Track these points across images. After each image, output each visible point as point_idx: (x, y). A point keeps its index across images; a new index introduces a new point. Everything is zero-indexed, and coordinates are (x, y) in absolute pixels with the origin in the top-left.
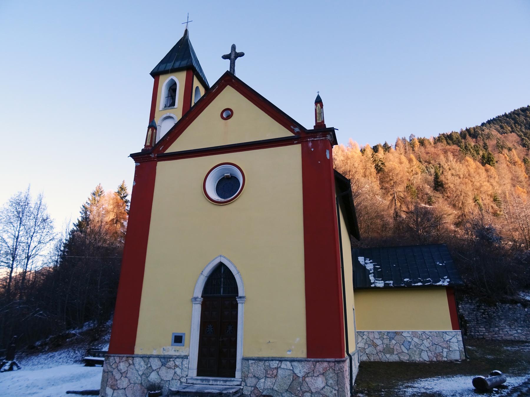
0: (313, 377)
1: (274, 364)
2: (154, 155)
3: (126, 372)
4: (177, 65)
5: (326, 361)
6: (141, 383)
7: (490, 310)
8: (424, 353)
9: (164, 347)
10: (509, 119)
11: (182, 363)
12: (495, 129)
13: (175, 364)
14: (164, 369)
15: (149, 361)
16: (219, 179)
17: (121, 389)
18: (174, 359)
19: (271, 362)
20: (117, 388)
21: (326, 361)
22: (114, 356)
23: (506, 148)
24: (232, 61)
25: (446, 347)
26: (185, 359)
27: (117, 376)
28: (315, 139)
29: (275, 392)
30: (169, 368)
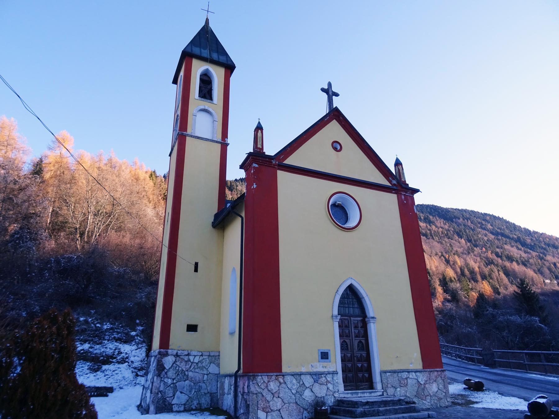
1: (405, 375)
2: (275, 162)
3: (278, 391)
9: (312, 364)
11: (332, 378)
13: (327, 380)
14: (316, 385)
17: (275, 411)
19: (402, 373)
22: (261, 376)
27: (269, 397)
30: (321, 385)
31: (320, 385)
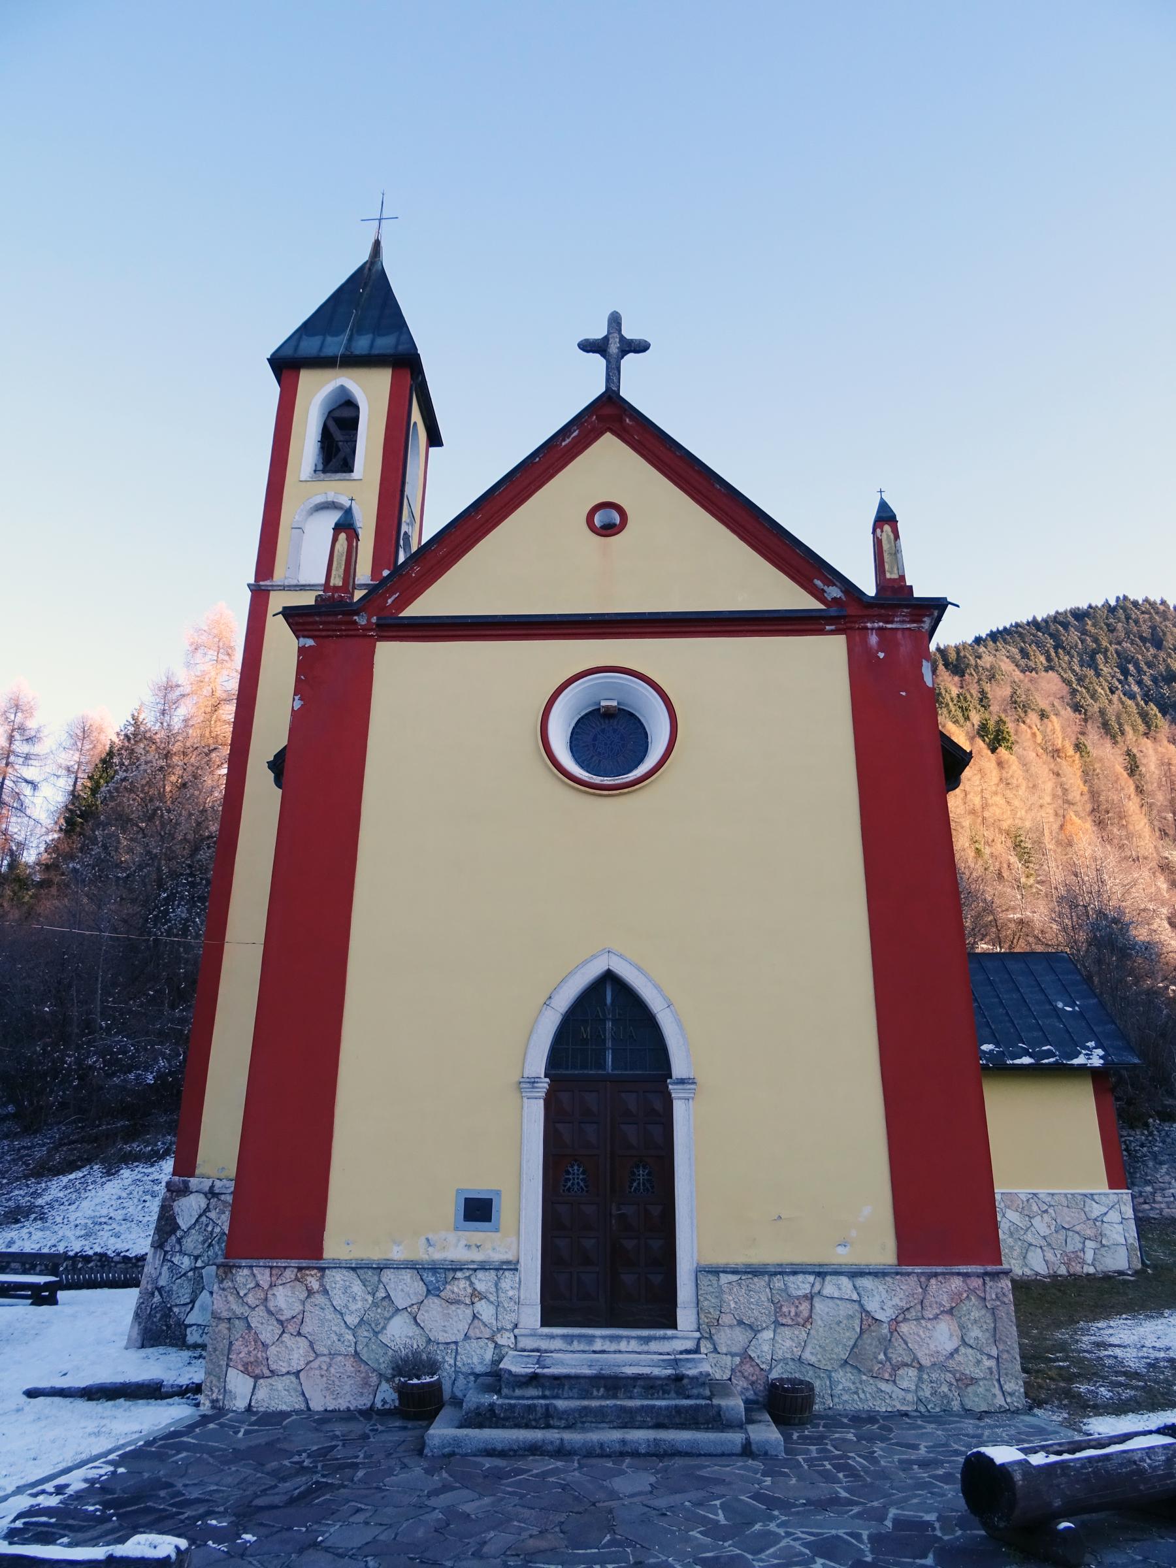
0: (922, 1321)
1: (801, 1285)
2: (369, 620)
3: (300, 1317)
4: (362, 345)
5: (959, 1274)
6: (356, 1351)
7: (1132, 1139)
8: (1034, 1252)
9: (430, 1237)
10: (1044, 634)
11: (496, 1285)
12: (1008, 657)
13: (475, 1289)
14: (434, 1303)
15: (380, 1281)
16: (579, 714)
17: (283, 1375)
18: (471, 1272)
19: (792, 1278)
20: (267, 1373)
21: (959, 1274)
22: (251, 1267)
23: (1033, 709)
24: (613, 361)
25: (1092, 1235)
26: (507, 1273)
27: (268, 1331)
28: (889, 626)
29: (808, 1368)
30: (451, 1303)
31: (445, 1304)
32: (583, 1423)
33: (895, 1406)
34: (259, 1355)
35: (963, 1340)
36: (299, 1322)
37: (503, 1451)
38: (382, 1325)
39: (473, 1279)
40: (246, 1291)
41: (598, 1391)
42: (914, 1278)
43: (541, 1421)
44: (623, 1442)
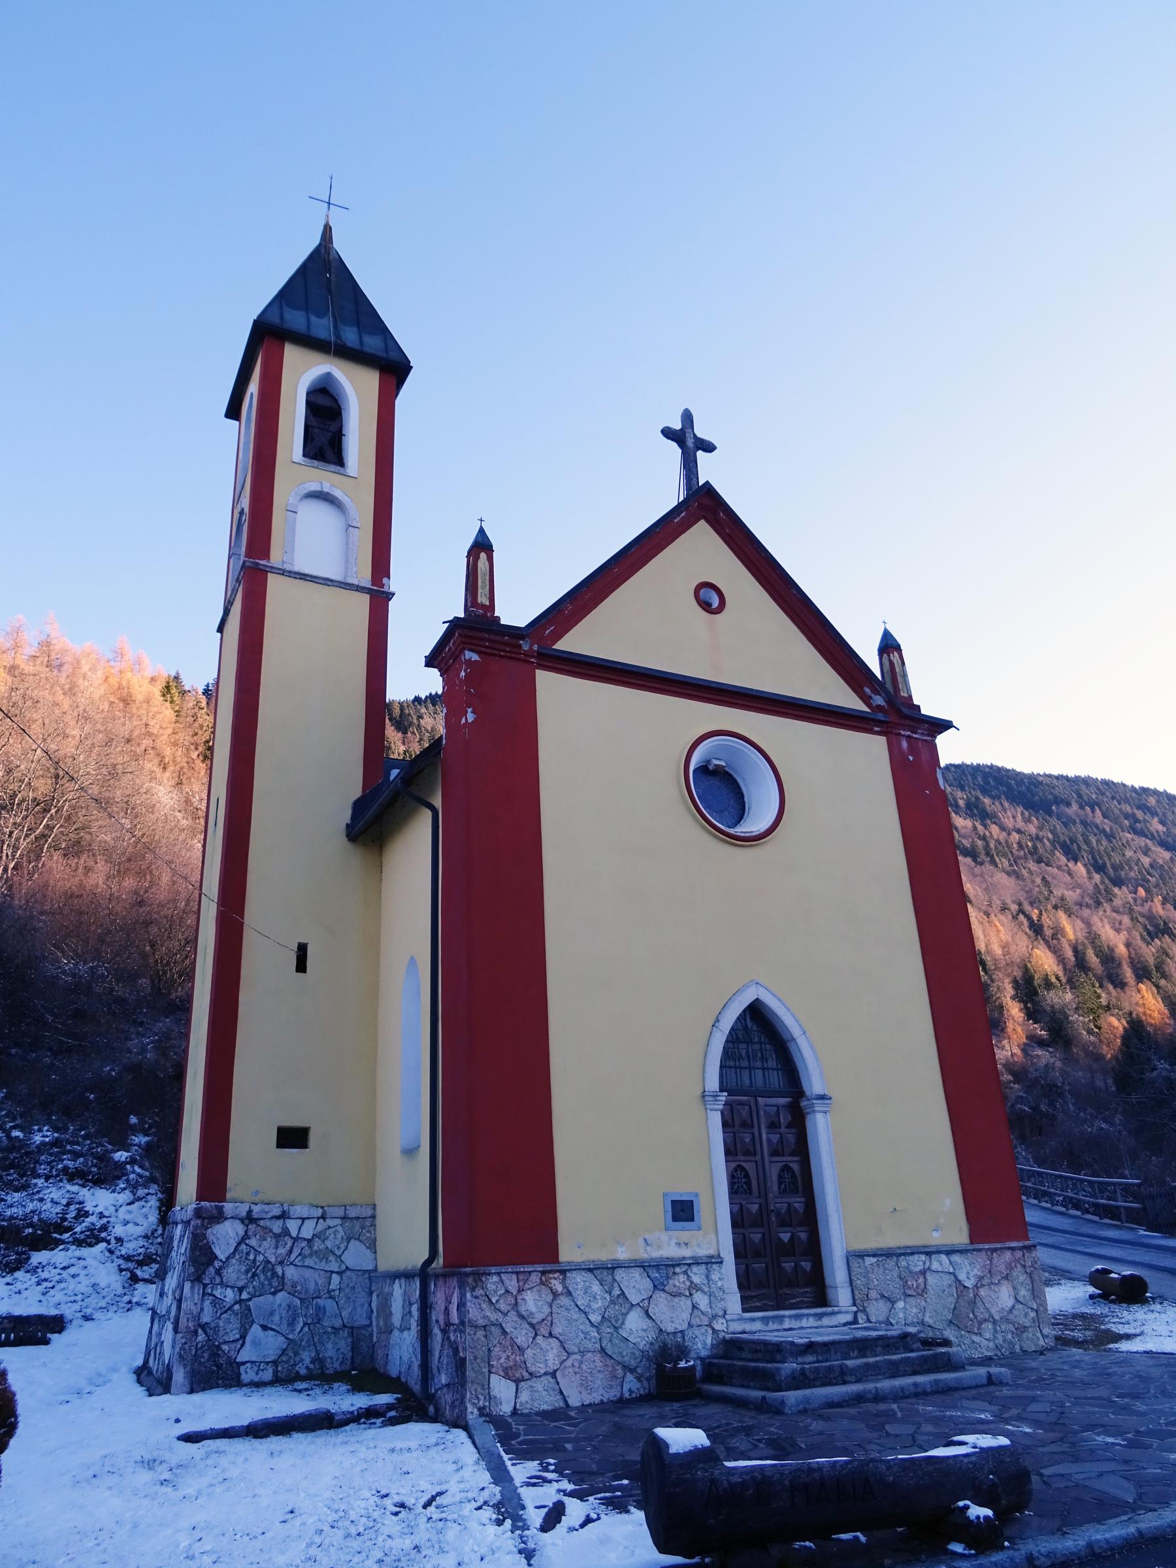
2: (531, 647)
3: (549, 1319)
6: (601, 1347)
11: (707, 1277)
13: (692, 1282)
14: (660, 1298)
15: (614, 1280)
17: (540, 1376)
19: (911, 1258)
21: (1009, 1248)
22: (499, 1274)
26: (715, 1266)
27: (522, 1336)
28: (914, 736)
30: (674, 1296)
31: (670, 1298)
32: (867, 1376)
33: (983, 1353)
34: (518, 1358)
35: (1016, 1298)
36: (549, 1324)
37: (839, 1402)
38: (621, 1320)
39: (689, 1273)
40: (497, 1298)
41: (853, 1352)
42: (984, 1252)
43: (839, 1379)
44: (916, 1385)
